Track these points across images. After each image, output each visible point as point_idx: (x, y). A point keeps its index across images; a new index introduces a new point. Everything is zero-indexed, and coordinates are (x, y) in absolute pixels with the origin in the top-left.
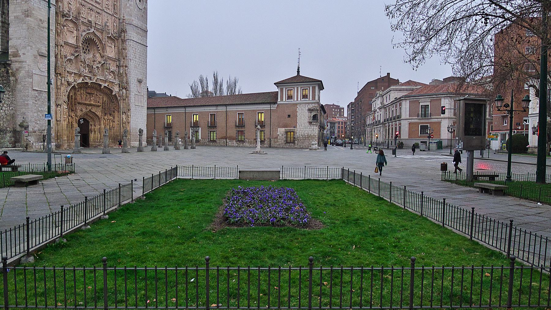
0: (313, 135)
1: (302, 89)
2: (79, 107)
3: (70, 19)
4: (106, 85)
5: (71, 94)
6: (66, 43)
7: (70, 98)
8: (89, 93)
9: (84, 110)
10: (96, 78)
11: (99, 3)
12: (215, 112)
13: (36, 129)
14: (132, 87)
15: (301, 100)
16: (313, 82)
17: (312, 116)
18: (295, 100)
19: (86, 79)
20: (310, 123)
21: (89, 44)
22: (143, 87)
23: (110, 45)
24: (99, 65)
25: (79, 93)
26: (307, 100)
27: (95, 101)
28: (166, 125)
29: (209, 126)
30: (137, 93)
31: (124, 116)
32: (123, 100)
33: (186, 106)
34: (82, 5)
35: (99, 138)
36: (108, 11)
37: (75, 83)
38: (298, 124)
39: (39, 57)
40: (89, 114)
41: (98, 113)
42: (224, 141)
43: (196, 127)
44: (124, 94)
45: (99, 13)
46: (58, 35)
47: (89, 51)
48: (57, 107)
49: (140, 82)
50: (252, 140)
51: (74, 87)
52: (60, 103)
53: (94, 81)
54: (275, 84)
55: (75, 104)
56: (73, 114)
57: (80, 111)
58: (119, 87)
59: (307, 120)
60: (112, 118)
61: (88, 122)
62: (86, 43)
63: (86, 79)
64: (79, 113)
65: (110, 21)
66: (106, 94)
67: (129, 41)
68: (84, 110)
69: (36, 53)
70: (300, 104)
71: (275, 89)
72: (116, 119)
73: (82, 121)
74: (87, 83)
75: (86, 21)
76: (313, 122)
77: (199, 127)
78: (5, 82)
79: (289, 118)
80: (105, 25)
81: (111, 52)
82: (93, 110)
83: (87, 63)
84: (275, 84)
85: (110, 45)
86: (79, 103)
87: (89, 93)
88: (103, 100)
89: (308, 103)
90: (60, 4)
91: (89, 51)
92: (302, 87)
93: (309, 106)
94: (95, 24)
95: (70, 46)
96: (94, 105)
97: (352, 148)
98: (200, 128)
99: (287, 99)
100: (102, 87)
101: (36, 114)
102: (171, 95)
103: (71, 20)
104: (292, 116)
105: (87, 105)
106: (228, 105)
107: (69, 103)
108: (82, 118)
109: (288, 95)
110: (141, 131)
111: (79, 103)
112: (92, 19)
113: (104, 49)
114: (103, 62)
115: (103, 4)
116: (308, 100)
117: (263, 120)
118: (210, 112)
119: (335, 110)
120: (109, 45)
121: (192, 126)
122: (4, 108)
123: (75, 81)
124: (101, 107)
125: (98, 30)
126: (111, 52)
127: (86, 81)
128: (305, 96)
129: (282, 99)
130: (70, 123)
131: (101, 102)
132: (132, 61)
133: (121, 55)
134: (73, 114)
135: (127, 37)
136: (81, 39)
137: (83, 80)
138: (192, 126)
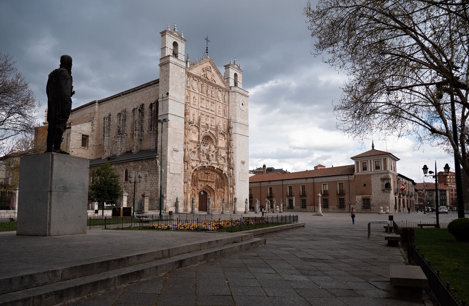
0: (386, 201)
1: (375, 161)
2: (199, 183)
3: (194, 125)
4: (218, 167)
5: (194, 175)
6: (191, 141)
7: (194, 177)
8: (206, 173)
9: (203, 185)
10: (211, 163)
11: (213, 111)
12: (304, 184)
13: (171, 198)
14: (237, 168)
15: (374, 170)
16: (386, 154)
17: (385, 184)
18: (369, 171)
19: (204, 164)
20: (383, 191)
21: (207, 139)
22: (246, 167)
23: (221, 139)
24: (214, 154)
25: (200, 173)
26: (379, 170)
27: (211, 179)
28: (301, 194)
29: (338, 194)
30: (241, 172)
31: (231, 189)
32: (231, 177)
33: (283, 180)
34: (202, 114)
35: (213, 205)
36: (220, 115)
37: (196, 167)
38: (372, 192)
39: (174, 152)
40: (206, 188)
41: (213, 187)
42: (313, 208)
43: (291, 196)
44: (231, 173)
45: (213, 118)
46: (186, 136)
47: (207, 144)
48: (185, 183)
49: (243, 163)
50: (335, 206)
51: (196, 170)
52: (186, 181)
53: (210, 165)
54: (351, 158)
55: (197, 181)
56: (195, 188)
57: (201, 185)
58: (228, 168)
59: (380, 188)
60: (223, 190)
61: (207, 193)
62: (205, 139)
63: (204, 164)
64: (200, 187)
65: (221, 122)
66: (219, 173)
67: (235, 134)
68: (203, 185)
69: (172, 150)
70: (374, 174)
71: (353, 163)
72: (226, 191)
73: (202, 193)
74: (205, 166)
75: (205, 124)
76: (385, 190)
77: (293, 196)
78: (155, 169)
79: (365, 187)
80: (218, 125)
81: (222, 143)
82: (209, 185)
83: (205, 153)
84: (351, 158)
85: (221, 139)
86: (200, 181)
87: (206, 173)
88: (216, 178)
89: (381, 174)
90: (187, 116)
91: (207, 144)
92: (362, 161)
93: (381, 176)
94: (211, 125)
95: (194, 142)
96: (210, 182)
97: (417, 212)
98: (294, 197)
99: (363, 171)
100: (215, 169)
101: (171, 189)
102: (286, 171)
103: (195, 126)
104: (367, 185)
105: (205, 182)
106: (315, 177)
107: (193, 181)
108: (203, 191)
109: (363, 167)
110: (246, 199)
111: (200, 181)
112: (209, 122)
113: (217, 142)
114: (216, 151)
115: (217, 111)
116: (380, 170)
117: (327, 189)
118: (301, 184)
119: (450, 177)
120: (220, 139)
121: (288, 195)
122: (154, 185)
123: (196, 166)
124: (215, 183)
125: (212, 129)
126: (222, 143)
127: (204, 165)
128: (377, 168)
129: (358, 171)
130: (194, 194)
131: (215, 179)
132: (237, 149)
133: (229, 145)
134: (196, 188)
135: (233, 132)
136: (201, 137)
137: (202, 165)
138: (288, 195)
